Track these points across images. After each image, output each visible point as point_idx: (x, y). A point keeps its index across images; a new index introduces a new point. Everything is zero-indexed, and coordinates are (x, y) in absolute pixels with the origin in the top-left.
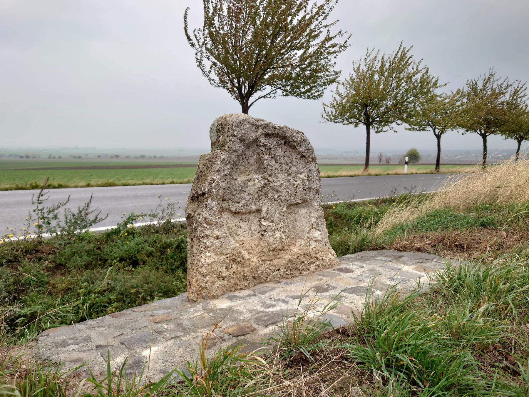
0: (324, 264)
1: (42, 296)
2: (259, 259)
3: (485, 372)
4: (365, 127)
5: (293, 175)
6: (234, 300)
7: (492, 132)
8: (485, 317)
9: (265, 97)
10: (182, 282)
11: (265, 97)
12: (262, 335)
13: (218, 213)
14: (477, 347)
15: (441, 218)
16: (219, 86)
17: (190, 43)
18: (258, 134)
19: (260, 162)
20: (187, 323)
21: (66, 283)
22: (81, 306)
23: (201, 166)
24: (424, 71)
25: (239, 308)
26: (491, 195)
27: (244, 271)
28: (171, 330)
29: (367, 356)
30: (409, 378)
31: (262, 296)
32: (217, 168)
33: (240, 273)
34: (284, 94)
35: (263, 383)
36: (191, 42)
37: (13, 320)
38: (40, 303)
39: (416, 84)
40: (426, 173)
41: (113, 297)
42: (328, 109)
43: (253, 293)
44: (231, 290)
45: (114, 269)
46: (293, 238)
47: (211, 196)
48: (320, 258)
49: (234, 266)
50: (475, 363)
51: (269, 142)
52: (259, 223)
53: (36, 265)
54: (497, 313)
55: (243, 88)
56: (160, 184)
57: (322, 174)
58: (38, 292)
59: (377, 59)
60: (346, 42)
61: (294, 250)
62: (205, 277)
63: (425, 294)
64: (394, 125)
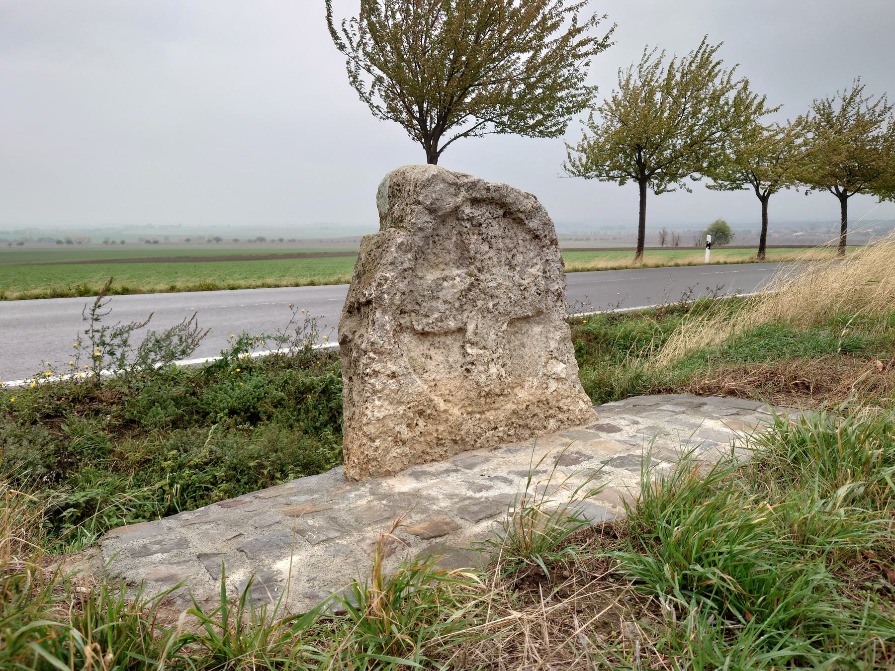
0: (571, 417)
1: (103, 472)
2: (463, 410)
3: (849, 597)
4: (637, 185)
5: (518, 269)
6: (422, 478)
7: (858, 190)
8: (848, 505)
9: (466, 135)
10: (333, 449)
11: (466, 135)
12: (470, 536)
13: (394, 335)
14: (836, 556)
15: (770, 338)
16: (388, 118)
17: (336, 44)
18: (459, 199)
19: (463, 247)
20: (345, 517)
21: (142, 451)
22: (167, 488)
23: (363, 256)
24: (741, 85)
25: (430, 492)
26: (855, 298)
27: (437, 430)
28: (320, 529)
29: (648, 571)
30: (721, 607)
31: (468, 471)
32: (390, 259)
33: (431, 434)
34: (499, 129)
35: (476, 616)
36: (339, 41)
37: (58, 512)
38: (100, 485)
39: (726, 109)
40: (742, 263)
41: (220, 473)
42: (575, 155)
43: (454, 467)
44: (416, 461)
45: (221, 427)
46: (519, 376)
47: (380, 305)
48: (565, 408)
49: (421, 423)
50: (832, 583)
51: (478, 213)
52: (462, 351)
53: (90, 422)
54: (869, 500)
55: (429, 119)
56: (292, 285)
57: (568, 266)
58: (95, 465)
59: (660, 67)
60: (607, 37)
61: (520, 396)
62: (374, 441)
63: (745, 467)
64: (687, 180)
